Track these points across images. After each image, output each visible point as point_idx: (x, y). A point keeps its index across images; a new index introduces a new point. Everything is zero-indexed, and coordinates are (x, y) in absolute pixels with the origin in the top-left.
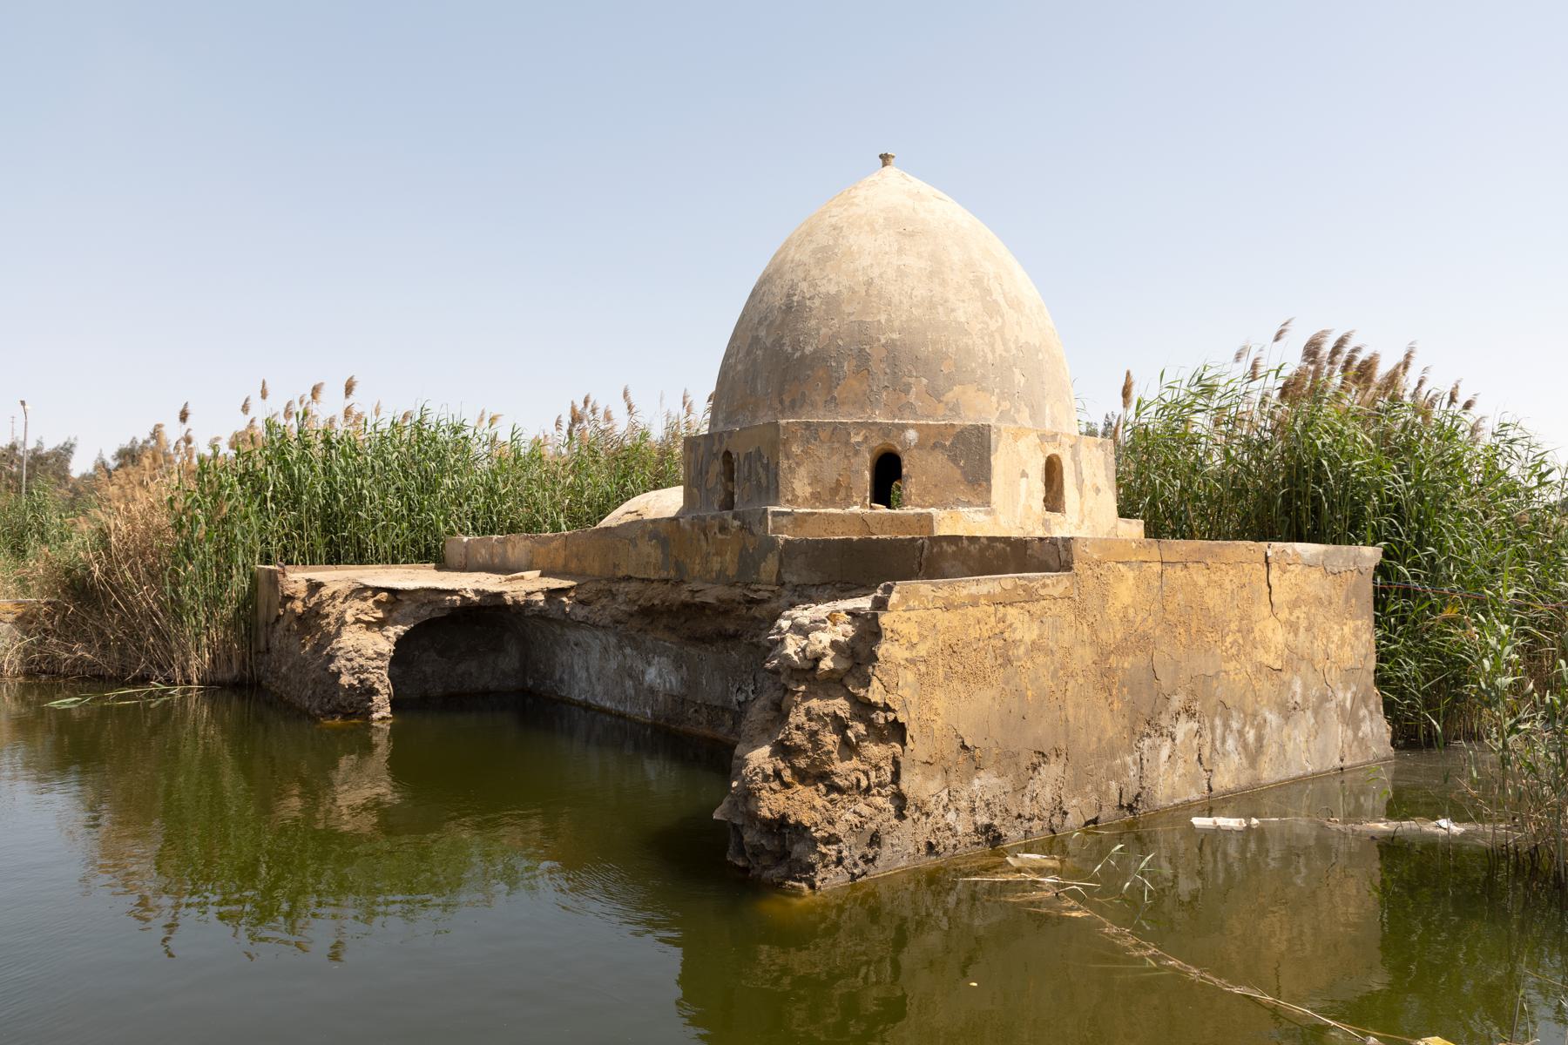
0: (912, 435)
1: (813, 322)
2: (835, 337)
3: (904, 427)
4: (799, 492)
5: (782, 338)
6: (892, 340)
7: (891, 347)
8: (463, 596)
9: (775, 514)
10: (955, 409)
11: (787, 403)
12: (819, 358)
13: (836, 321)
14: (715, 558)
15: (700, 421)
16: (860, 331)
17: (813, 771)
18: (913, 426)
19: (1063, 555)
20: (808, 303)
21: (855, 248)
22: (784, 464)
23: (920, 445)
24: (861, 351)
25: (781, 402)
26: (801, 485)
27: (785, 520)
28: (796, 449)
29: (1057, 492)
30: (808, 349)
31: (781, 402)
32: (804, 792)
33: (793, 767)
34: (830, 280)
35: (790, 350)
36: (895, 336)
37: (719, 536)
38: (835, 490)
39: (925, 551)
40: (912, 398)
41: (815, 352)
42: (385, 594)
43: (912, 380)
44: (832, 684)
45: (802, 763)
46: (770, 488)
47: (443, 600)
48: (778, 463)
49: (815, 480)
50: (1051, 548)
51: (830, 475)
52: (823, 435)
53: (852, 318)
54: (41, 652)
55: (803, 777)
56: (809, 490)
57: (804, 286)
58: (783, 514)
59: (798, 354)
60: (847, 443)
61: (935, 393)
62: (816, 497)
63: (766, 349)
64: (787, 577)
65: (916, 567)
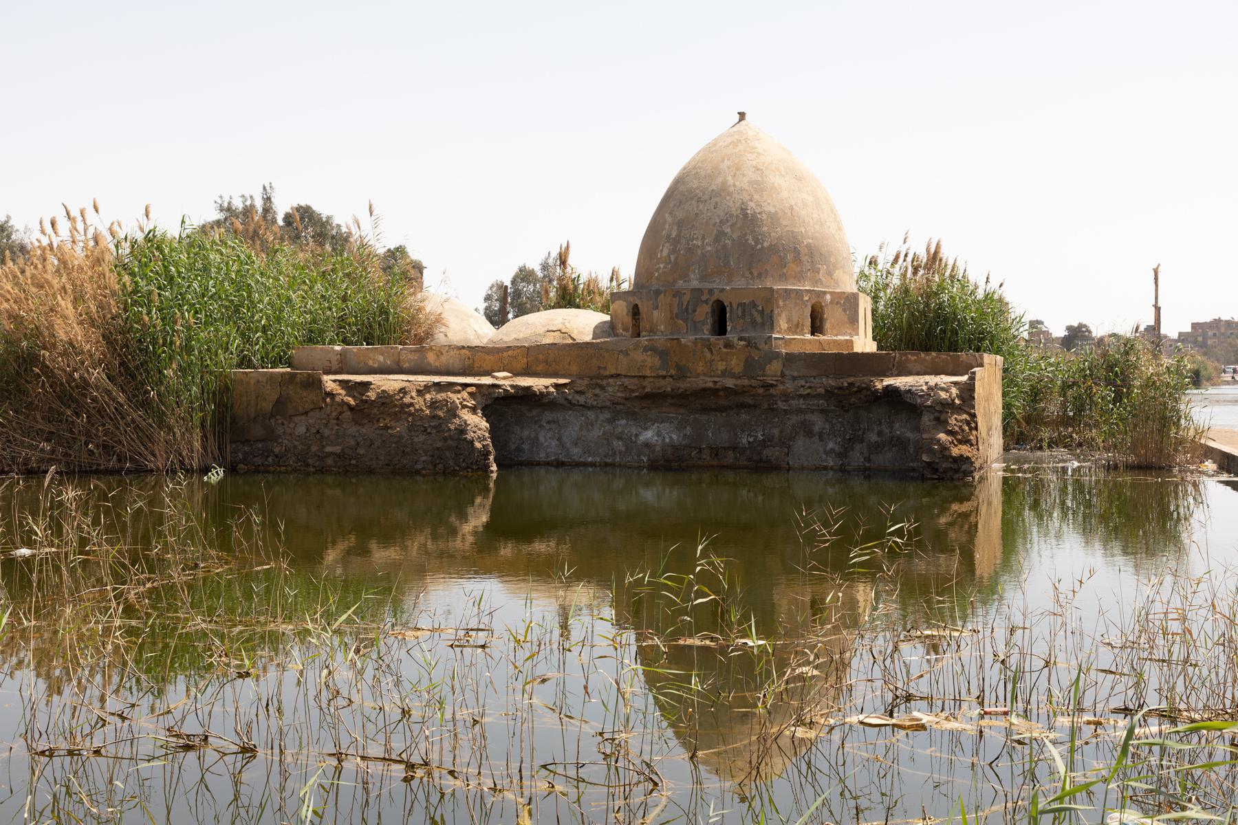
0: (828, 297)
1: (765, 229)
2: (779, 239)
3: (825, 293)
4: (782, 327)
5: (746, 235)
6: (810, 243)
7: (809, 246)
8: (504, 389)
9: (776, 339)
10: (837, 283)
11: (755, 274)
12: (773, 249)
13: (778, 229)
14: (720, 363)
15: (628, 273)
16: (794, 237)
17: (964, 440)
18: (829, 292)
19: (979, 360)
20: (759, 216)
21: (776, 185)
22: (776, 312)
23: (831, 303)
24: (795, 248)
25: (751, 273)
26: (783, 323)
27: (780, 342)
28: (781, 303)
29: (1203, 347)
30: (766, 244)
31: (751, 273)
32: (964, 447)
33: (956, 439)
34: (769, 204)
35: (753, 243)
36: (810, 241)
37: (725, 350)
38: (797, 326)
39: (897, 359)
40: (821, 276)
41: (771, 245)
42: (474, 388)
43: (820, 266)
44: (959, 409)
45: (960, 437)
46: (768, 322)
47: (495, 392)
48: (772, 311)
49: (789, 320)
50: (972, 358)
51: (795, 317)
52: (793, 295)
53: (788, 228)
54: (701, 404)
55: (960, 442)
56: (786, 325)
57: (752, 204)
58: (779, 339)
59: (759, 246)
60: (802, 300)
61: (830, 274)
62: (789, 330)
63: (734, 240)
64: (787, 373)
65: (891, 366)
